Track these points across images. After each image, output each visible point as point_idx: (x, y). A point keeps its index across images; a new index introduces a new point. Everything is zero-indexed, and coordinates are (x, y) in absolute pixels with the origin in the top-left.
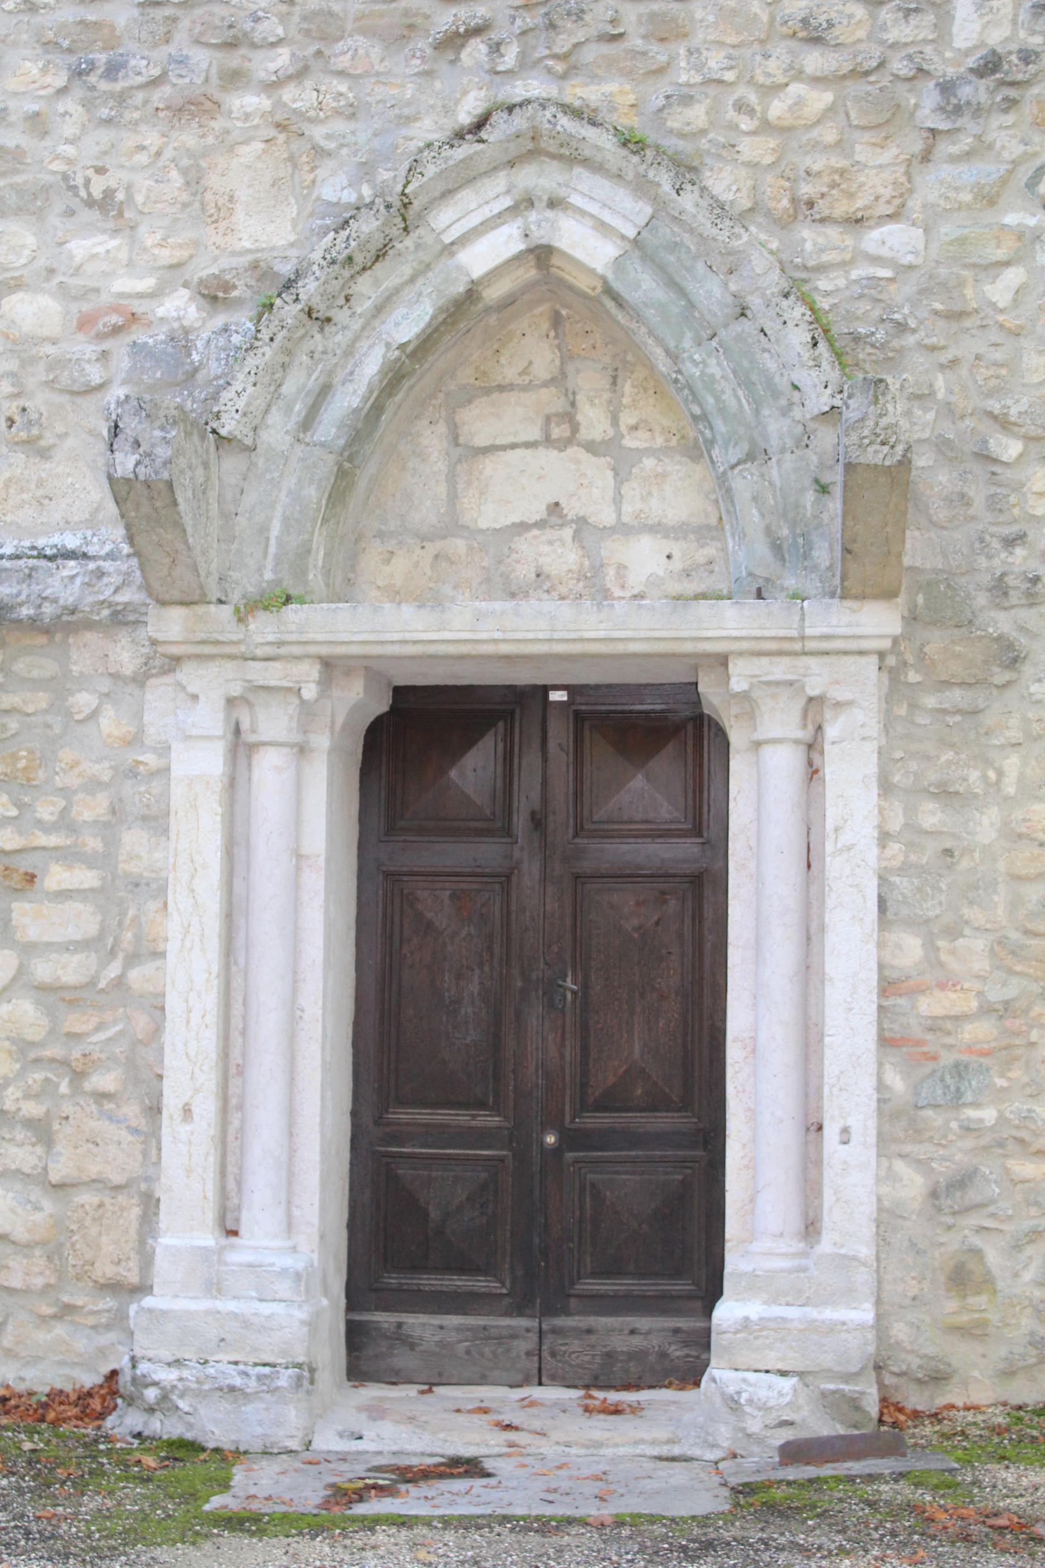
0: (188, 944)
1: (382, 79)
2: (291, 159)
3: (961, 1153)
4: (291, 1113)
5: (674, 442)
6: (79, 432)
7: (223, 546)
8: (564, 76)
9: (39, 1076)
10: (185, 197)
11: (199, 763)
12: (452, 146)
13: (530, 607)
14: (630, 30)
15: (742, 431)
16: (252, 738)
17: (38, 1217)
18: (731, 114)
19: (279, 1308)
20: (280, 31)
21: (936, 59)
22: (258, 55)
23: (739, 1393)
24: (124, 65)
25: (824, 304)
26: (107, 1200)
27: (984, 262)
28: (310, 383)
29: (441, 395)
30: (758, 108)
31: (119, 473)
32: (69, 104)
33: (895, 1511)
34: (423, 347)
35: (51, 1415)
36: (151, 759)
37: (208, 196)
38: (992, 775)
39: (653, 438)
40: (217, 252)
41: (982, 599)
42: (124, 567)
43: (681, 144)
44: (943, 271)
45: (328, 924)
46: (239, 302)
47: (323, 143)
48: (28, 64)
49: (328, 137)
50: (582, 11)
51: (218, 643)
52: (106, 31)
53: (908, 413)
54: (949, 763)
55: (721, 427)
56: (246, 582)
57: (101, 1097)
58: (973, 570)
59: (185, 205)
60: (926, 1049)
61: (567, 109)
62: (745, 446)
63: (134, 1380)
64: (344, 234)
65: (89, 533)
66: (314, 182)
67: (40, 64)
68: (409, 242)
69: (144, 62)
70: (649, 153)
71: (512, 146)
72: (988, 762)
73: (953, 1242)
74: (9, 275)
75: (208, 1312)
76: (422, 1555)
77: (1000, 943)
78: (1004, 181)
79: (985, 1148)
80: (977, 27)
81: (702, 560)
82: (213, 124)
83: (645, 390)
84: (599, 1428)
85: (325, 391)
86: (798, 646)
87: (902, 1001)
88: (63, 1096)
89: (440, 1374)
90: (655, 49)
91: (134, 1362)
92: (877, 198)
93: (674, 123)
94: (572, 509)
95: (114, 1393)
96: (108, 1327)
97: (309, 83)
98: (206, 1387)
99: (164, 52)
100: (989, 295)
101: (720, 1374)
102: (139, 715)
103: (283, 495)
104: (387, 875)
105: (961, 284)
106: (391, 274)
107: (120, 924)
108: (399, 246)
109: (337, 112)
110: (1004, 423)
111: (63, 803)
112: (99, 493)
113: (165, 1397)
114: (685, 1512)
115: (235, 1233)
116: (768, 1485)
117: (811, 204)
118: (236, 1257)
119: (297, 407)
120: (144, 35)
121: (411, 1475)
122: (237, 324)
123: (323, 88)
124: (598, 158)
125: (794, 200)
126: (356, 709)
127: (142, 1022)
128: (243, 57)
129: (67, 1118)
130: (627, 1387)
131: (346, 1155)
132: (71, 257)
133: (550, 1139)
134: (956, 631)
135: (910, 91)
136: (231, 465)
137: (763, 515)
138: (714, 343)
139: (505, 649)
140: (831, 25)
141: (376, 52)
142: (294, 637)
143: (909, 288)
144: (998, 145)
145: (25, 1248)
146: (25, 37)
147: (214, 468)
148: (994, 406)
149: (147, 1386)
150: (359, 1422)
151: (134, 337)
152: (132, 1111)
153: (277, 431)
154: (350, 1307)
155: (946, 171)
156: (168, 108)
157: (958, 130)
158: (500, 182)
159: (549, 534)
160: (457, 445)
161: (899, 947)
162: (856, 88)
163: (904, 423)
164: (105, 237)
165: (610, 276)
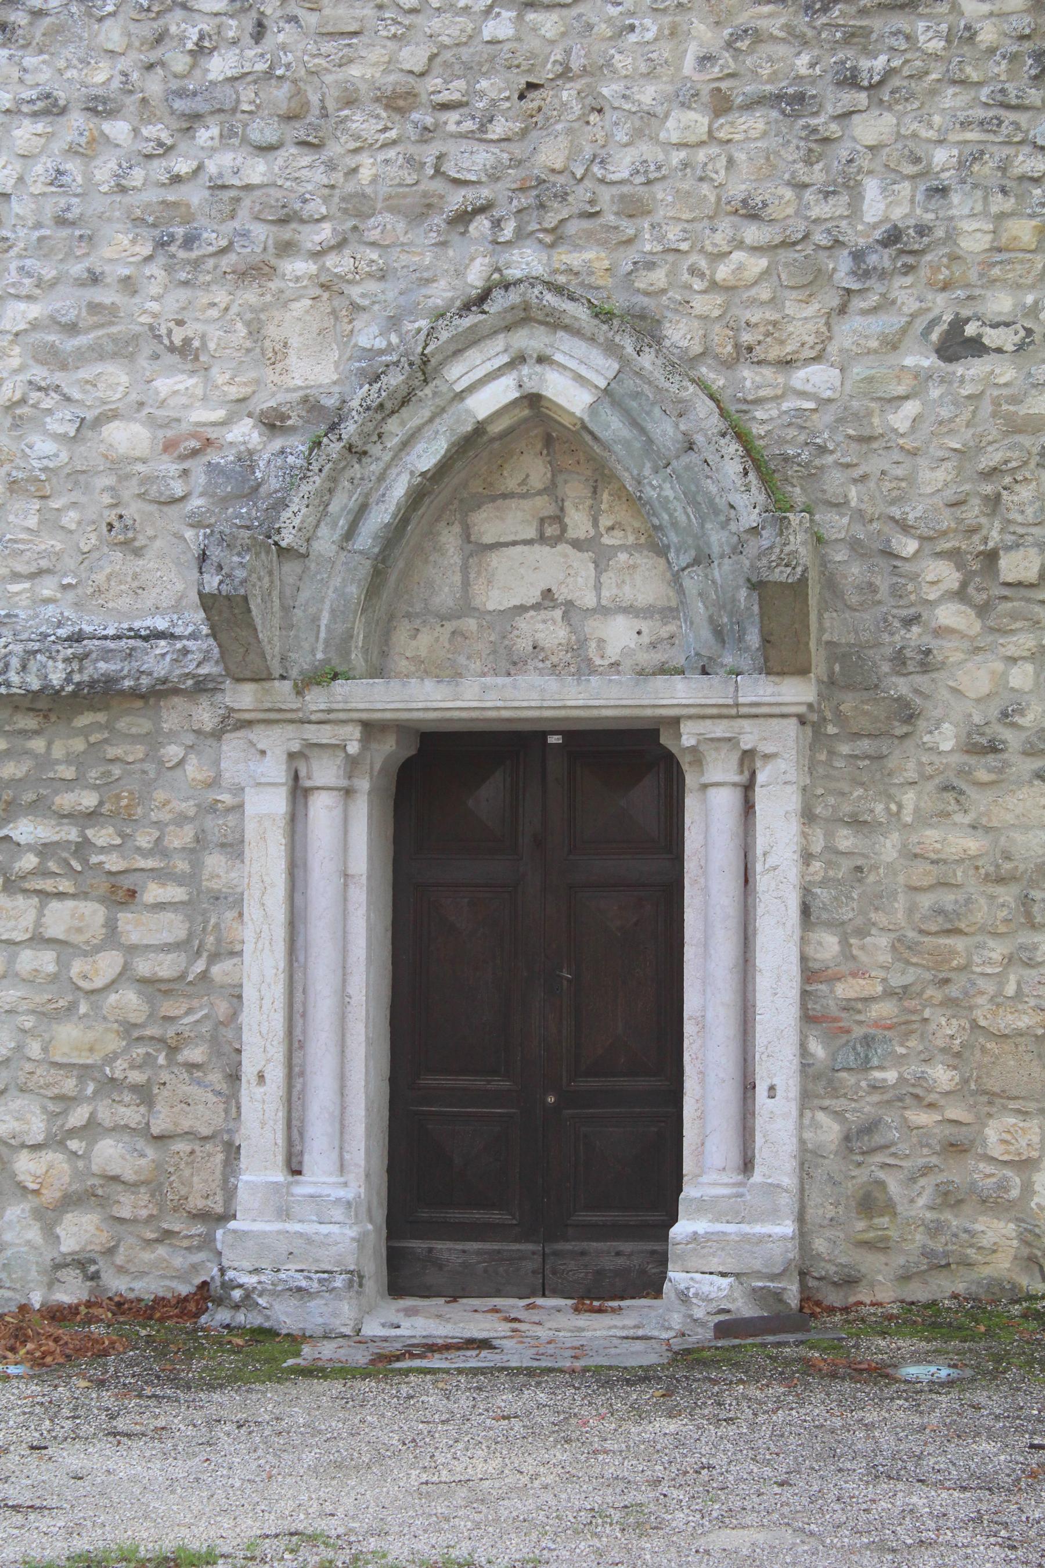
0: (260, 946)
1: (406, 248)
2: (334, 312)
3: (869, 1106)
4: (342, 1078)
5: (642, 540)
7: (284, 633)
8: (552, 246)
9: (141, 1051)
10: (248, 344)
11: (267, 805)
12: (461, 316)
14: (605, 207)
15: (690, 541)
16: (308, 784)
17: (143, 1162)
18: (686, 277)
19: (335, 1229)
20: (324, 210)
21: (849, 231)
22: (306, 229)
23: (688, 1288)
26: (197, 1148)
27: (888, 396)
28: (351, 504)
29: (456, 502)
30: (708, 272)
31: (207, 590)
32: (154, 269)
33: (788, 1362)
34: (443, 468)
35: (158, 1315)
36: (227, 798)
37: (267, 343)
38: (894, 807)
39: (626, 537)
40: (275, 389)
41: (886, 668)
42: (205, 646)
43: (646, 301)
44: (855, 404)
45: (370, 929)
46: (293, 429)
47: (359, 301)
48: (121, 236)
49: (363, 296)
50: (566, 194)
51: (280, 710)
52: (183, 209)
54: (860, 797)
56: (302, 662)
57: (191, 1067)
58: (878, 645)
59: (248, 351)
60: (841, 1024)
62: (693, 553)
63: (223, 1285)
64: (376, 386)
65: (175, 617)
66: (352, 331)
67: (131, 236)
68: (428, 391)
69: (214, 235)
71: (509, 316)
73: (862, 1176)
74: (107, 407)
75: (279, 1232)
76: (441, 1385)
77: (899, 940)
78: (904, 331)
79: (888, 1102)
80: (882, 206)
81: (666, 635)
82: (270, 284)
83: (620, 498)
84: (583, 1320)
85: (363, 509)
86: (733, 711)
87: (823, 987)
88: (161, 1067)
89: (463, 1289)
90: (625, 224)
91: (222, 1271)
92: (803, 345)
93: (640, 285)
94: (562, 594)
96: (199, 1248)
97: (347, 252)
98: (279, 1288)
100: (892, 423)
101: (676, 1276)
102: (217, 763)
103: (330, 592)
105: (869, 414)
106: (414, 417)
107: (204, 929)
108: (420, 394)
109: (370, 275)
111: (157, 834)
113: (247, 1296)
114: (634, 1364)
115: (299, 1173)
117: (750, 349)
118: (298, 1190)
119: (341, 523)
120: (213, 213)
121: (432, 1348)
122: (291, 447)
123: (359, 256)
124: (576, 325)
125: (737, 346)
127: (222, 1008)
128: (294, 230)
129: (164, 1084)
131: (386, 1113)
132: (157, 393)
133: (551, 1099)
134: (865, 693)
135: (829, 257)
136: (290, 569)
137: (707, 608)
138: (669, 471)
140: (765, 205)
141: (401, 226)
142: (340, 706)
143: (823, 420)
144: (899, 302)
146: (117, 214)
147: (276, 573)
148: (896, 512)
149: (233, 1288)
151: (209, 458)
152: (215, 1078)
153: (325, 542)
154: (389, 1237)
156: (234, 272)
157: (867, 289)
158: (499, 342)
159: (544, 614)
160: (469, 542)
161: (820, 943)
162: (785, 256)
164: (184, 377)
165: (586, 419)
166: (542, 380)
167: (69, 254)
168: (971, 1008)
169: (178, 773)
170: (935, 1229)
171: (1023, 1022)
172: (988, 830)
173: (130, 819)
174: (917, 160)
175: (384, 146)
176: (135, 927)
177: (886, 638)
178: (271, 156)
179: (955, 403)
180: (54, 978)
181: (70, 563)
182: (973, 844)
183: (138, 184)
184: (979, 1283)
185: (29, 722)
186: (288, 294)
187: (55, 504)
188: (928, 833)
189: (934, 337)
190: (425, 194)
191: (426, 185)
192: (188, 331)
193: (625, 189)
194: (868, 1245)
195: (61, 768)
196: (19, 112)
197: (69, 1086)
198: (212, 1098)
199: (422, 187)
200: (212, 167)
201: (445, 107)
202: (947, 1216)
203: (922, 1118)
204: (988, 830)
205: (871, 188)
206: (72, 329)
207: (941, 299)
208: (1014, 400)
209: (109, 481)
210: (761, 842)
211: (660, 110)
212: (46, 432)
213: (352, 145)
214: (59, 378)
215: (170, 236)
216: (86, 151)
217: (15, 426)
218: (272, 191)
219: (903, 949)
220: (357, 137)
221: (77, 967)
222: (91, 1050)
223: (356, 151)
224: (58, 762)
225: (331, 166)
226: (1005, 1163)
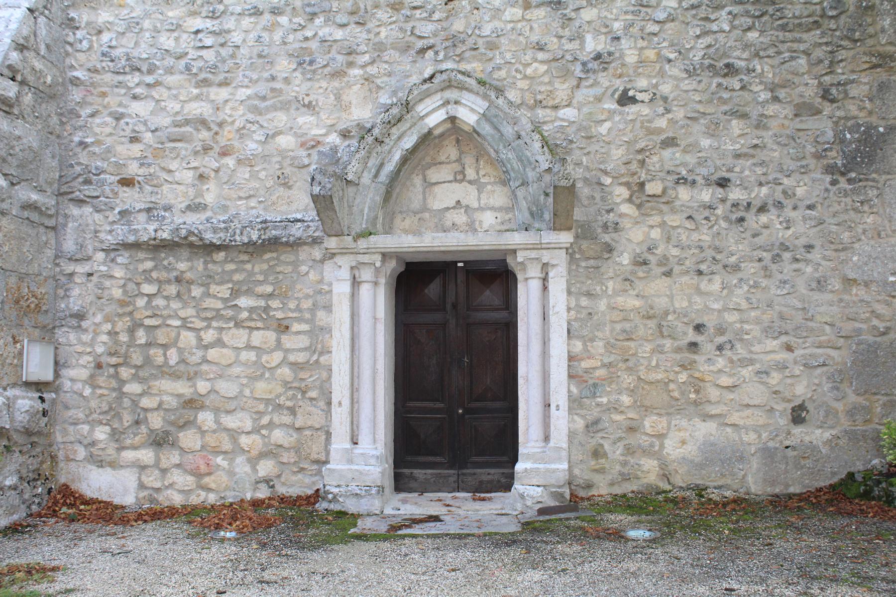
4: (374, 403)
6: (301, 181)
8: (459, 62)
10: (335, 103)
11: (342, 289)
13: (450, 235)
16: (359, 280)
17: (292, 439)
18: (514, 73)
19: (371, 468)
20: (366, 49)
22: (358, 57)
24: (315, 61)
25: (546, 134)
36: (326, 287)
38: (604, 288)
41: (599, 230)
43: (498, 83)
44: (584, 123)
45: (385, 341)
46: (353, 136)
49: (382, 82)
53: (574, 169)
55: (513, 175)
56: (357, 229)
57: (312, 399)
58: (596, 221)
61: (463, 73)
68: (409, 116)
70: (487, 86)
72: (603, 284)
73: (593, 442)
76: (420, 546)
78: (604, 94)
84: (478, 505)
85: (382, 165)
86: (539, 246)
87: (576, 363)
91: (324, 486)
94: (464, 202)
95: (318, 496)
96: (316, 475)
97: (375, 65)
99: (327, 57)
101: (517, 486)
102: (322, 273)
104: (405, 325)
105: (590, 127)
106: (403, 126)
109: (385, 75)
110: (606, 173)
112: (308, 200)
113: (335, 497)
116: (534, 522)
117: (541, 102)
126: (393, 270)
127: (325, 375)
130: (487, 492)
131: (393, 418)
133: (460, 411)
136: (351, 190)
139: (442, 249)
140: (546, 44)
141: (397, 55)
145: (288, 449)
148: (602, 167)
150: (399, 504)
152: (322, 404)
153: (366, 179)
154: (395, 468)
155: (584, 91)
158: (438, 96)
159: (457, 211)
163: (573, 173)
166: (456, 110)
167: (263, 69)
168: (637, 371)
169: (306, 277)
170: (624, 464)
171: (660, 376)
172: (643, 297)
173: (286, 297)
174: (607, 26)
175: (390, 24)
176: (288, 341)
177: (600, 218)
178: (344, 29)
179: (626, 123)
180: (255, 363)
181: (262, 192)
182: (637, 303)
183: (291, 41)
184: (642, 486)
185: (245, 257)
186: (351, 83)
187: (256, 169)
188: (619, 298)
189: (616, 96)
190: (407, 42)
191: (407, 39)
192: (311, 98)
193: (488, 39)
194: (596, 471)
195: (258, 276)
196: (244, 14)
197: (261, 407)
198: (320, 412)
199: (406, 39)
200: (321, 34)
201: (415, 8)
202: (629, 458)
203: (618, 417)
204: (643, 297)
205: (589, 38)
206: (264, 98)
207: (618, 81)
208: (650, 121)
209: (279, 159)
210: (552, 302)
211: (502, 8)
212: (253, 140)
213: (378, 23)
214: (258, 118)
215: (304, 61)
216: (271, 28)
217: (241, 138)
218: (345, 42)
219: (609, 346)
220: (379, 20)
221: (265, 358)
222: (270, 392)
223: (379, 26)
224: (256, 273)
225: (369, 31)
226: (653, 435)
